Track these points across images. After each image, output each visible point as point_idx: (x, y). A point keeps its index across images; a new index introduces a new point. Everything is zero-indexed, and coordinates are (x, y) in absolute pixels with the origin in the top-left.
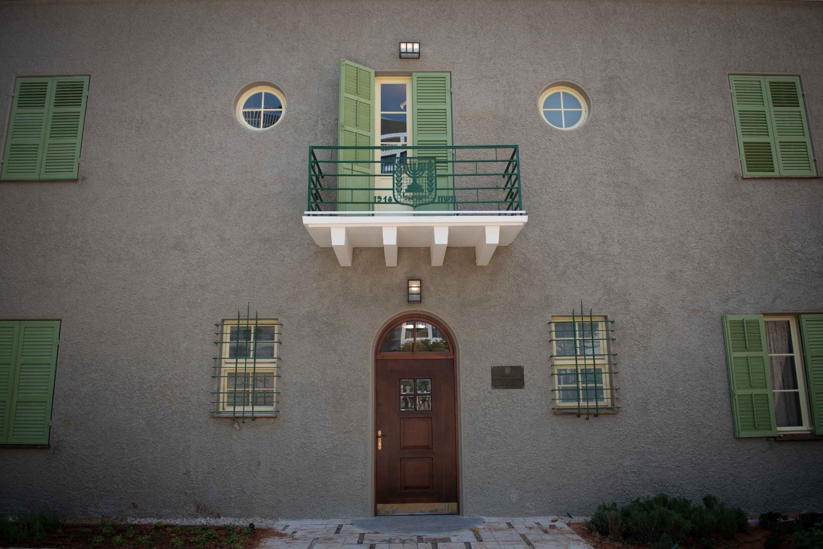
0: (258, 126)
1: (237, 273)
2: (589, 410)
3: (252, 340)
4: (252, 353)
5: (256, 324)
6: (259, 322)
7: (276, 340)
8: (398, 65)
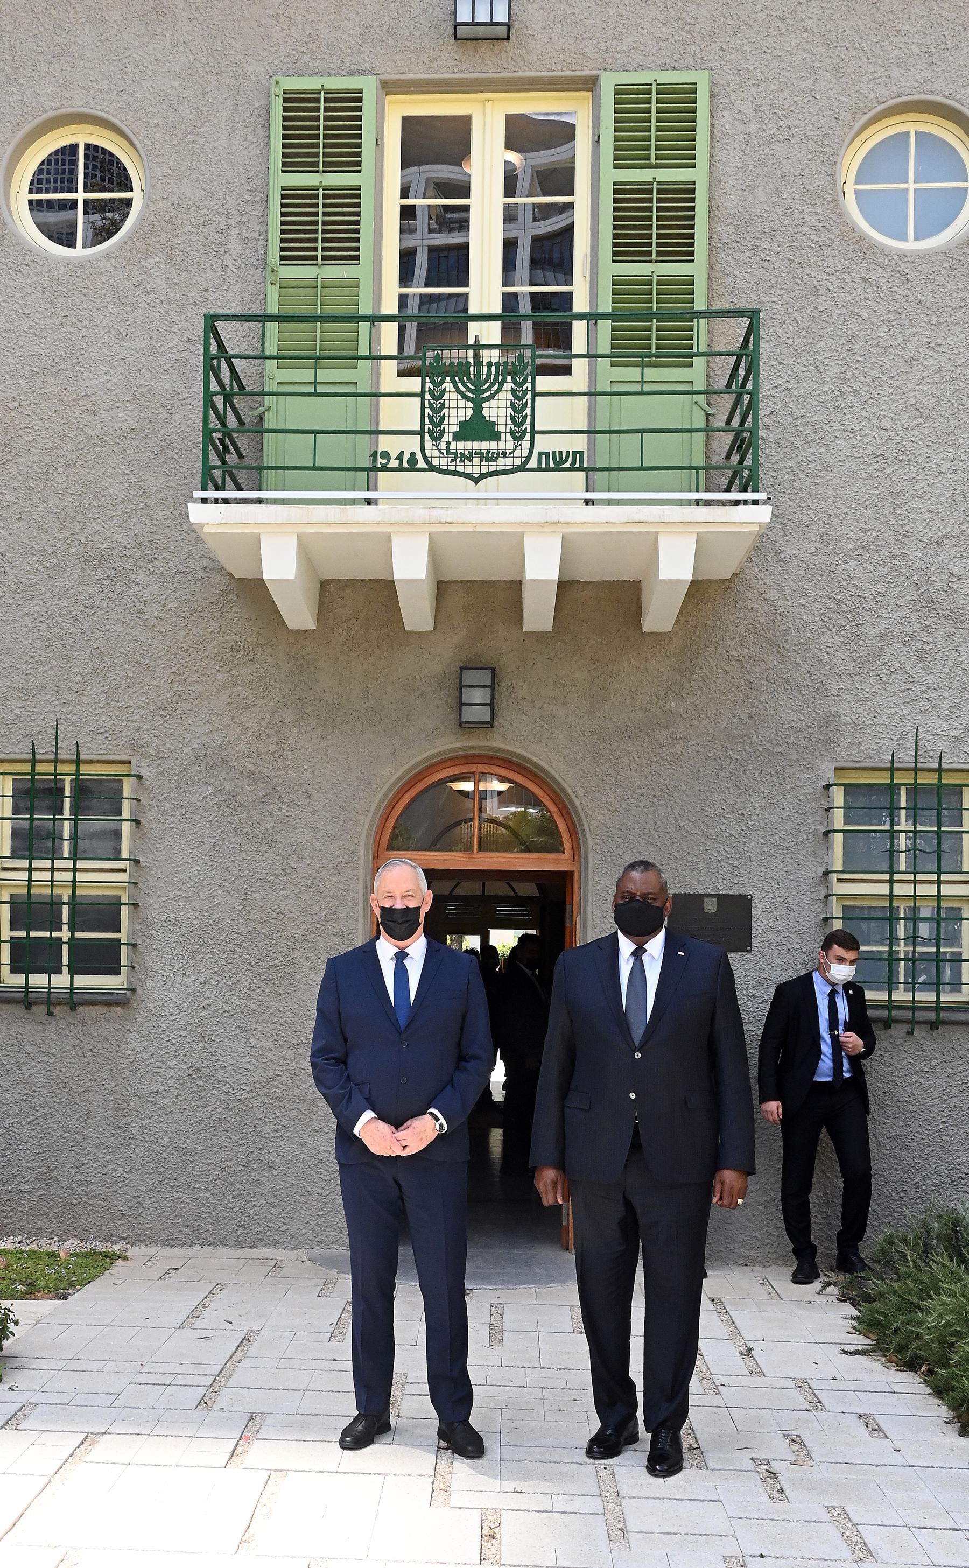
0: (71, 244)
1: (26, 642)
2: (917, 1013)
3: (67, 814)
4: (66, 846)
5: (78, 774)
6: (84, 768)
7: (126, 814)
8: (449, 62)
